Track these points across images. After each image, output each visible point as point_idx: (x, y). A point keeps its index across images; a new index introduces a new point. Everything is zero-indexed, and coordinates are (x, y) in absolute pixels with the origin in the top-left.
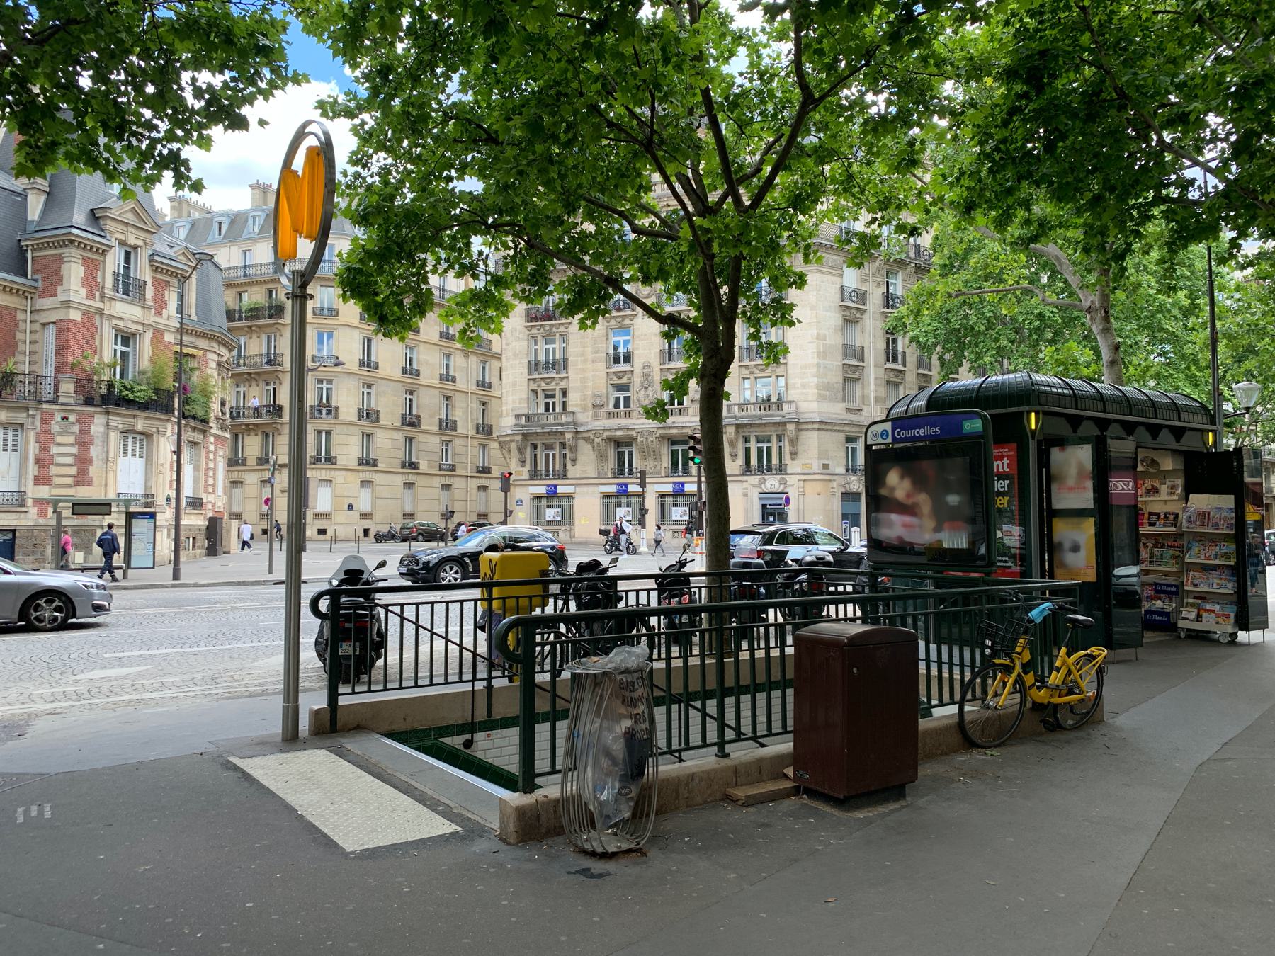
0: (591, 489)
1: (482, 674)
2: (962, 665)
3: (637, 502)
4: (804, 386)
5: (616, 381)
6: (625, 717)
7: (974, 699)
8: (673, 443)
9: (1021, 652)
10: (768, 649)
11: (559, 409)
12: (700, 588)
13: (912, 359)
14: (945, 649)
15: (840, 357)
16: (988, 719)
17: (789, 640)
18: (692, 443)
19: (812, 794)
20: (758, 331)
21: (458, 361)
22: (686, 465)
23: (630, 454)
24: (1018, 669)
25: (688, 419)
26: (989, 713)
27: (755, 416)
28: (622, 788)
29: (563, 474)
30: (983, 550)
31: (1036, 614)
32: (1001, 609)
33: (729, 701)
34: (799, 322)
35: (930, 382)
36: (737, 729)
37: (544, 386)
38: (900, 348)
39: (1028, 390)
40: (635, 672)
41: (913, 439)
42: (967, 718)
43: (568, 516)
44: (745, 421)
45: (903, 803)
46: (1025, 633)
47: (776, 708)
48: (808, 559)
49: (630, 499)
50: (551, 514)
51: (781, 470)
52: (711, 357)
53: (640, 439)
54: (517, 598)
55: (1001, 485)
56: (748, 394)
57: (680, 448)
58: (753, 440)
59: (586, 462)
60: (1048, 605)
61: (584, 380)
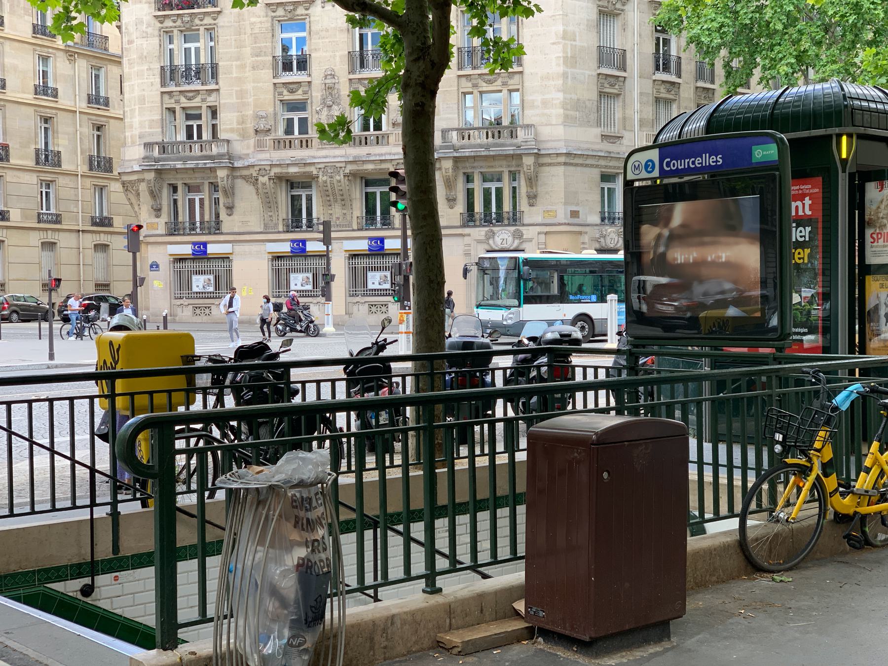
0: (254, 247)
1: (104, 493)
2: (744, 468)
3: (320, 264)
4: (545, 103)
5: (287, 96)
6: (299, 544)
7: (760, 509)
8: (368, 183)
9: (823, 448)
10: (493, 454)
11: (206, 135)
12: (404, 377)
13: (688, 68)
14: (722, 448)
15: (594, 63)
16: (776, 535)
17: (523, 443)
18: (393, 182)
19: (548, 634)
20: (482, 23)
21: (60, 66)
22: (385, 213)
23: (309, 199)
24: (817, 470)
25: (390, 151)
26: (778, 527)
27: (481, 146)
28: (293, 637)
29: (216, 227)
30: (774, 322)
31: (842, 400)
32: (797, 393)
33: (441, 524)
34: (540, 10)
35: (712, 100)
36: (452, 557)
37: (184, 102)
38: (674, 52)
39: (839, 106)
40: (313, 484)
41: (688, 171)
42: (751, 535)
43: (224, 284)
44: (467, 152)
45: (666, 644)
46: (828, 423)
47: (504, 531)
48: (549, 336)
49: (310, 261)
50: (199, 283)
51: (515, 219)
52: (417, 60)
53: (322, 178)
54: (151, 393)
55: (800, 234)
56: (470, 115)
57: (378, 190)
58: (477, 178)
59: (247, 211)
60: (856, 387)
61: (241, 94)
